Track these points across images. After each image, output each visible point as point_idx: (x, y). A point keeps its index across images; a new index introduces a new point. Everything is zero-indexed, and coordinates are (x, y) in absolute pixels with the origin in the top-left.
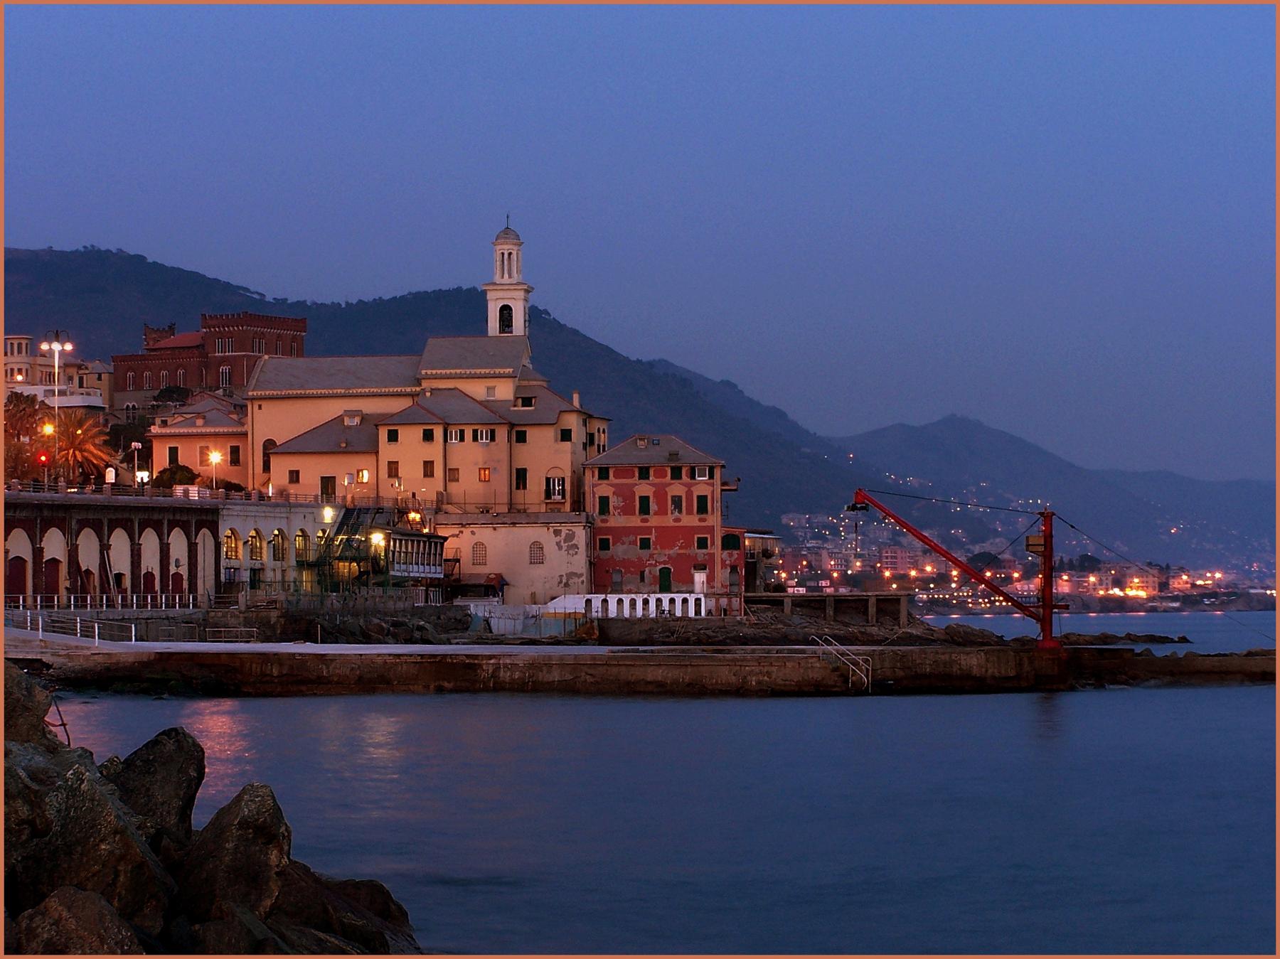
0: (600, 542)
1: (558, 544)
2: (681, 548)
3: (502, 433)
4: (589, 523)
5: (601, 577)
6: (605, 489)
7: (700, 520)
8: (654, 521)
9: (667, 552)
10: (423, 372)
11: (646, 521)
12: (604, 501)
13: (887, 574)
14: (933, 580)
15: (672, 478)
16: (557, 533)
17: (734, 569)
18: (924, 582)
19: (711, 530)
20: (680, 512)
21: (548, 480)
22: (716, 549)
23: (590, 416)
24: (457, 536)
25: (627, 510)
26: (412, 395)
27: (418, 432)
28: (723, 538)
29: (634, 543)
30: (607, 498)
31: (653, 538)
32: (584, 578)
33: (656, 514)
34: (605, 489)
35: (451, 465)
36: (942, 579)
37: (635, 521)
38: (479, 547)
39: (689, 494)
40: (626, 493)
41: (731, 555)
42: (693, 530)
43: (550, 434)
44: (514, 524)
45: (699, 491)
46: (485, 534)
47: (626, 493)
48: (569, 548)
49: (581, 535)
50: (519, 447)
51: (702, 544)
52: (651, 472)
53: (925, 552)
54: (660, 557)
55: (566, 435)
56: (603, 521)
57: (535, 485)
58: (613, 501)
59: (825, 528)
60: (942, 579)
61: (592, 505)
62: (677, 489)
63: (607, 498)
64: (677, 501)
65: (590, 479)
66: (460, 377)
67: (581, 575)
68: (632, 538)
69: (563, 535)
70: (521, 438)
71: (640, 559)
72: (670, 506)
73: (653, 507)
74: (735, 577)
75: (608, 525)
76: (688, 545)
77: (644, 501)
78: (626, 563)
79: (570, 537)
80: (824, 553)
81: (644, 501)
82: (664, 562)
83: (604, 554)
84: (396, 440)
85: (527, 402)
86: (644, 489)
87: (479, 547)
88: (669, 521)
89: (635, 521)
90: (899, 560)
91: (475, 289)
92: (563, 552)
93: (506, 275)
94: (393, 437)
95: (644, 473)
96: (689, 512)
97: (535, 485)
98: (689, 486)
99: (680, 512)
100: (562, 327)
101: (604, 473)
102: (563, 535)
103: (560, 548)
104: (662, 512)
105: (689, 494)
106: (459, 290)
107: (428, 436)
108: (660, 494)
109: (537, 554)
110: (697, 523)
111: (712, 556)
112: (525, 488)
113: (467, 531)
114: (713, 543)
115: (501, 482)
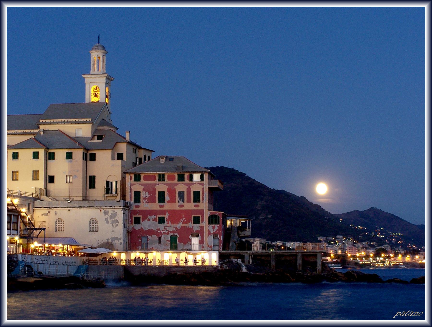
0: (134, 218)
1: (106, 220)
2: (183, 223)
3: (78, 154)
4: (126, 206)
5: (134, 240)
6: (138, 187)
7: (196, 206)
8: (167, 206)
9: (175, 225)
10: (41, 121)
11: (163, 206)
12: (137, 195)
13: (340, 252)
14: (364, 257)
15: (179, 180)
16: (106, 213)
17: (215, 235)
18: (361, 258)
19: (202, 212)
20: (183, 201)
21: (108, 183)
22: (205, 223)
23: (140, 148)
24: (47, 215)
25: (151, 200)
26: (33, 134)
27: (30, 152)
28: (209, 217)
29: (155, 220)
30: (139, 192)
31: (166, 217)
32: (122, 241)
33: (169, 202)
34: (138, 187)
35: (50, 174)
36: (367, 257)
37: (156, 206)
38: (59, 222)
39: (189, 190)
40: (151, 190)
41: (214, 228)
42: (192, 212)
43: (108, 154)
44: (80, 207)
45: (194, 188)
46: (63, 213)
47: (151, 190)
48: (113, 222)
49: (119, 212)
50: (91, 163)
51: (197, 220)
52: (166, 177)
53: (362, 248)
54: (170, 227)
55: (120, 156)
56: (136, 206)
57: (100, 185)
58: (144, 195)
59: (332, 241)
60: (367, 257)
61: (130, 198)
62: (181, 187)
63: (139, 192)
64: (181, 195)
65: (129, 181)
66: (61, 123)
67: (120, 239)
68: (154, 217)
69: (110, 214)
70: (93, 157)
71: (159, 229)
72: (177, 198)
73: (167, 198)
74: (217, 241)
75: (139, 209)
76: (188, 222)
77: (162, 194)
78: (151, 232)
79: (114, 215)
80: (329, 248)
81: (162, 194)
82: (173, 232)
83: (137, 227)
84: (17, 158)
85: (100, 137)
86: (161, 187)
87: (59, 222)
88: (176, 206)
89: (156, 206)
90: (353, 251)
91: (223, 167)
92: (109, 225)
93: (96, 70)
94: (15, 156)
95: (162, 178)
96: (189, 201)
97: (100, 185)
98: (189, 185)
99: (183, 201)
100: (250, 178)
101: (137, 178)
102: (110, 214)
103: (108, 222)
104: (172, 201)
105: (189, 190)
106: (218, 167)
107: (36, 156)
108: (171, 191)
109: (93, 226)
110: (159, 208)
111: (202, 228)
112: (94, 187)
113: (53, 211)
114: (203, 221)
115: (79, 183)
